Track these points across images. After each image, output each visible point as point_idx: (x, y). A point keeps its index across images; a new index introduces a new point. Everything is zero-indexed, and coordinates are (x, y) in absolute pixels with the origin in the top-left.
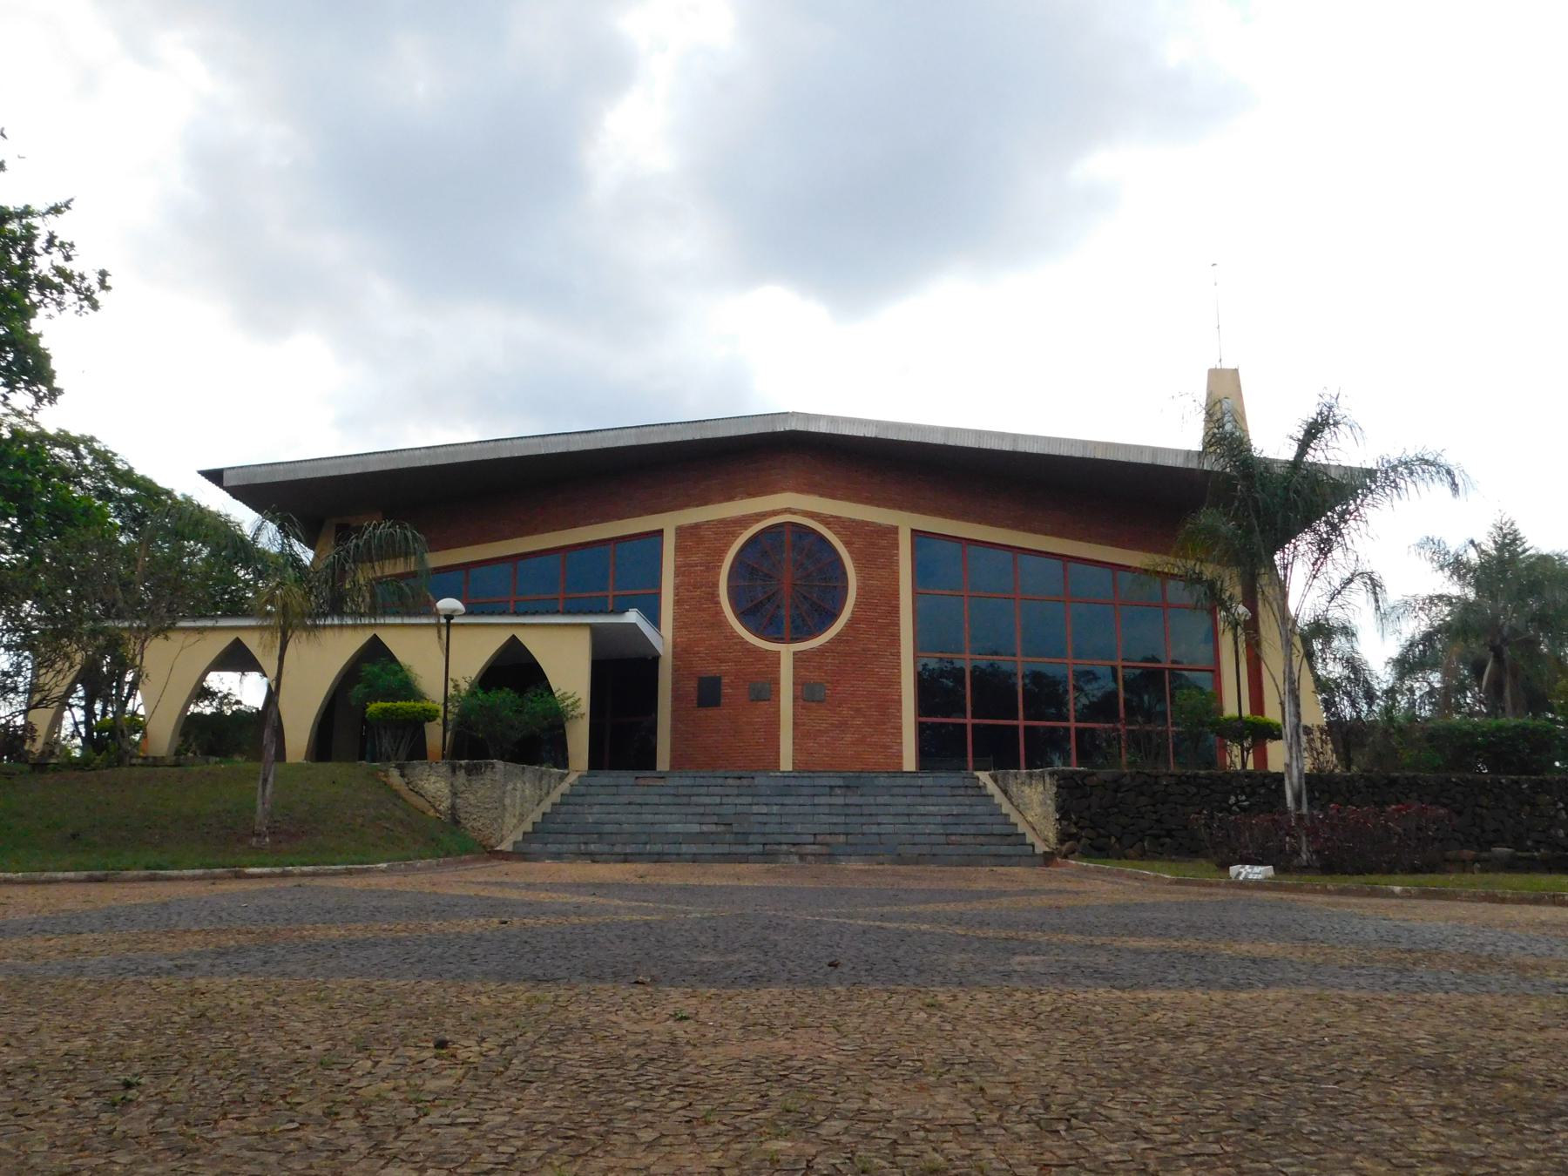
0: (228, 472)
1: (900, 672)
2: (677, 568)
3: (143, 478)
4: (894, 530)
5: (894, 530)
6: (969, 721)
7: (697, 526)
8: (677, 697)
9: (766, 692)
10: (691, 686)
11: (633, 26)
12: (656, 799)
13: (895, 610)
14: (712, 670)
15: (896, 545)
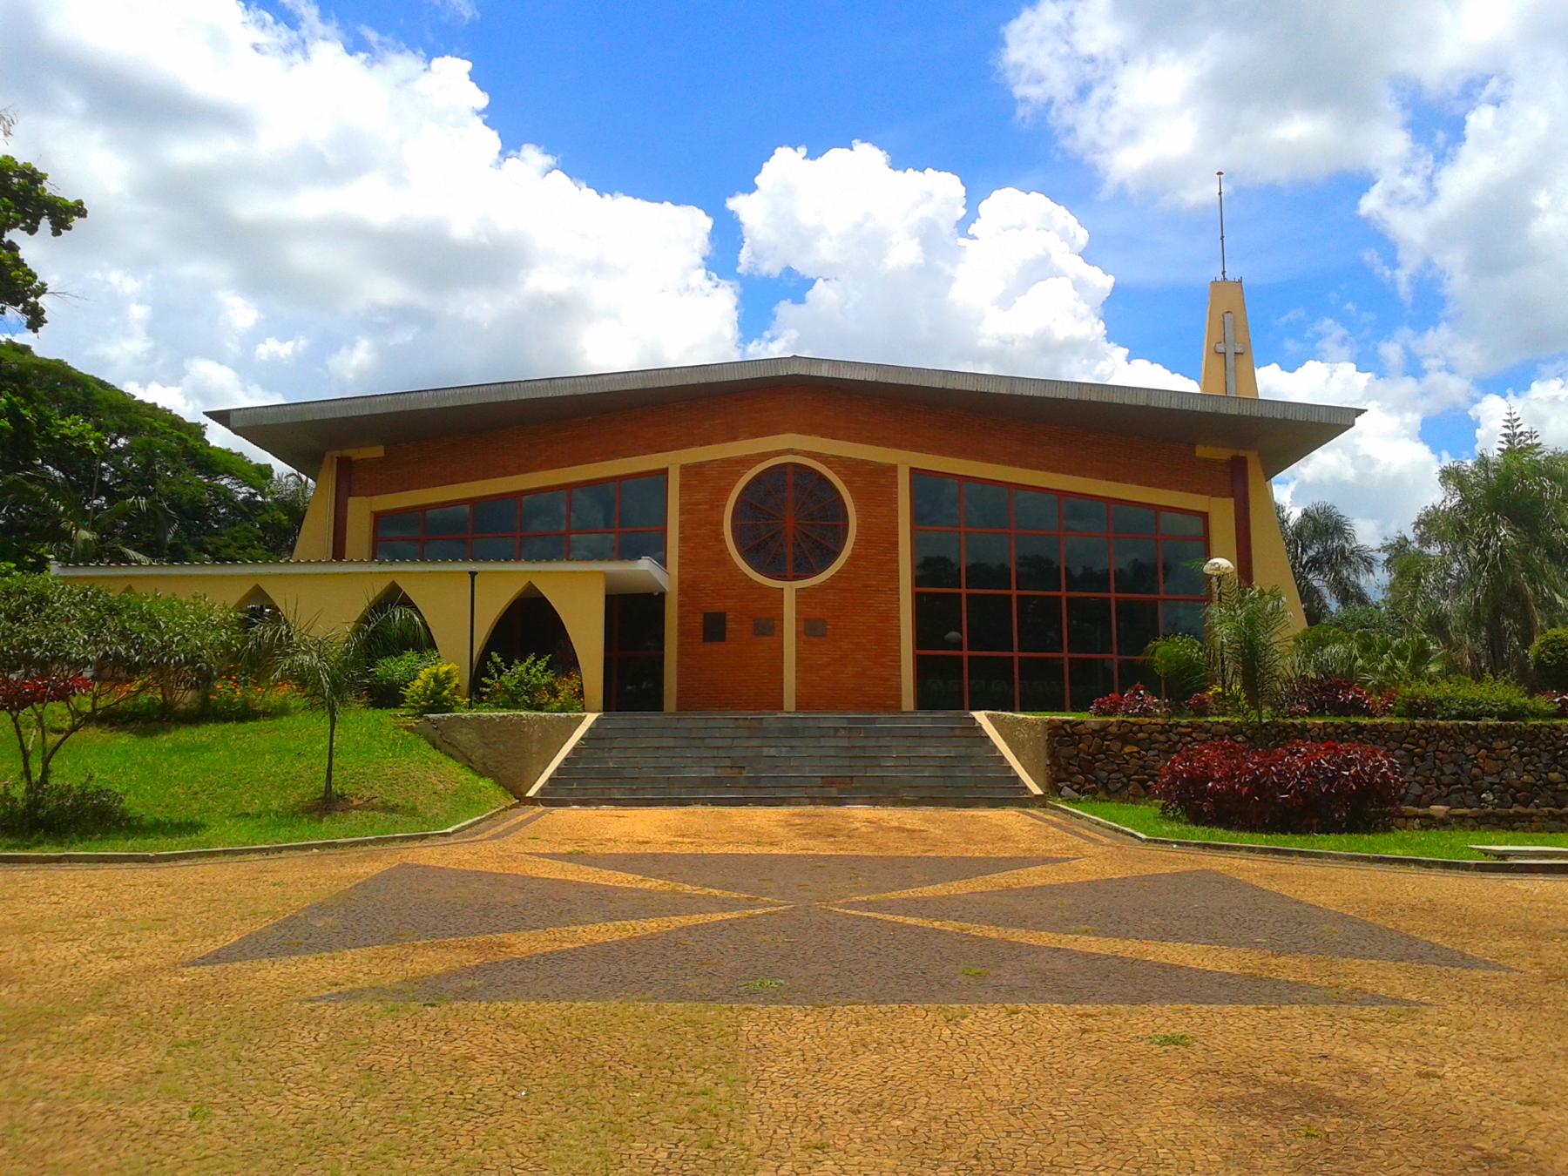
0: (235, 413)
1: (898, 607)
2: (682, 505)
3: (164, 410)
4: (894, 468)
5: (894, 468)
6: (1016, 654)
7: (701, 465)
8: (683, 633)
9: (769, 626)
10: (697, 621)
11: (3, 340)
12: (671, 743)
13: (894, 545)
14: (718, 606)
15: (895, 484)
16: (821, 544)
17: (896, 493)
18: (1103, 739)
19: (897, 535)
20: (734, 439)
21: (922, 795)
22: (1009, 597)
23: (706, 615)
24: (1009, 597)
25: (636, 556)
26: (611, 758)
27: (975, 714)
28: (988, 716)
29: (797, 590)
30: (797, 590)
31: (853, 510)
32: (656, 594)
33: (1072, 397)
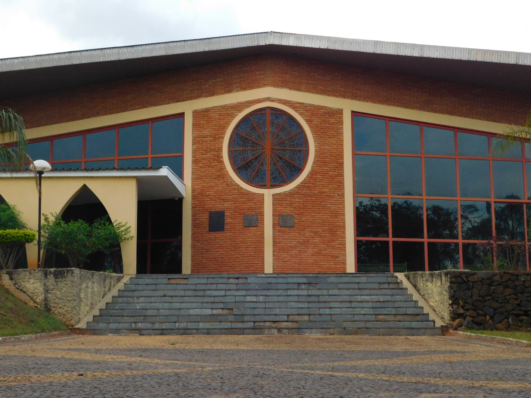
4: (340, 112)
5: (340, 112)
7: (207, 110)
8: (195, 225)
10: (205, 218)
12: (182, 293)
13: (341, 165)
14: (218, 207)
16: (290, 163)
17: (342, 128)
18: (490, 285)
19: (342, 158)
20: (230, 91)
21: (358, 326)
22: (423, 243)
23: (210, 213)
24: (423, 243)
25: (158, 168)
26: (138, 303)
27: (397, 274)
28: (406, 276)
29: (273, 195)
30: (273, 195)
31: (311, 136)
32: (177, 199)
33: (464, 58)
